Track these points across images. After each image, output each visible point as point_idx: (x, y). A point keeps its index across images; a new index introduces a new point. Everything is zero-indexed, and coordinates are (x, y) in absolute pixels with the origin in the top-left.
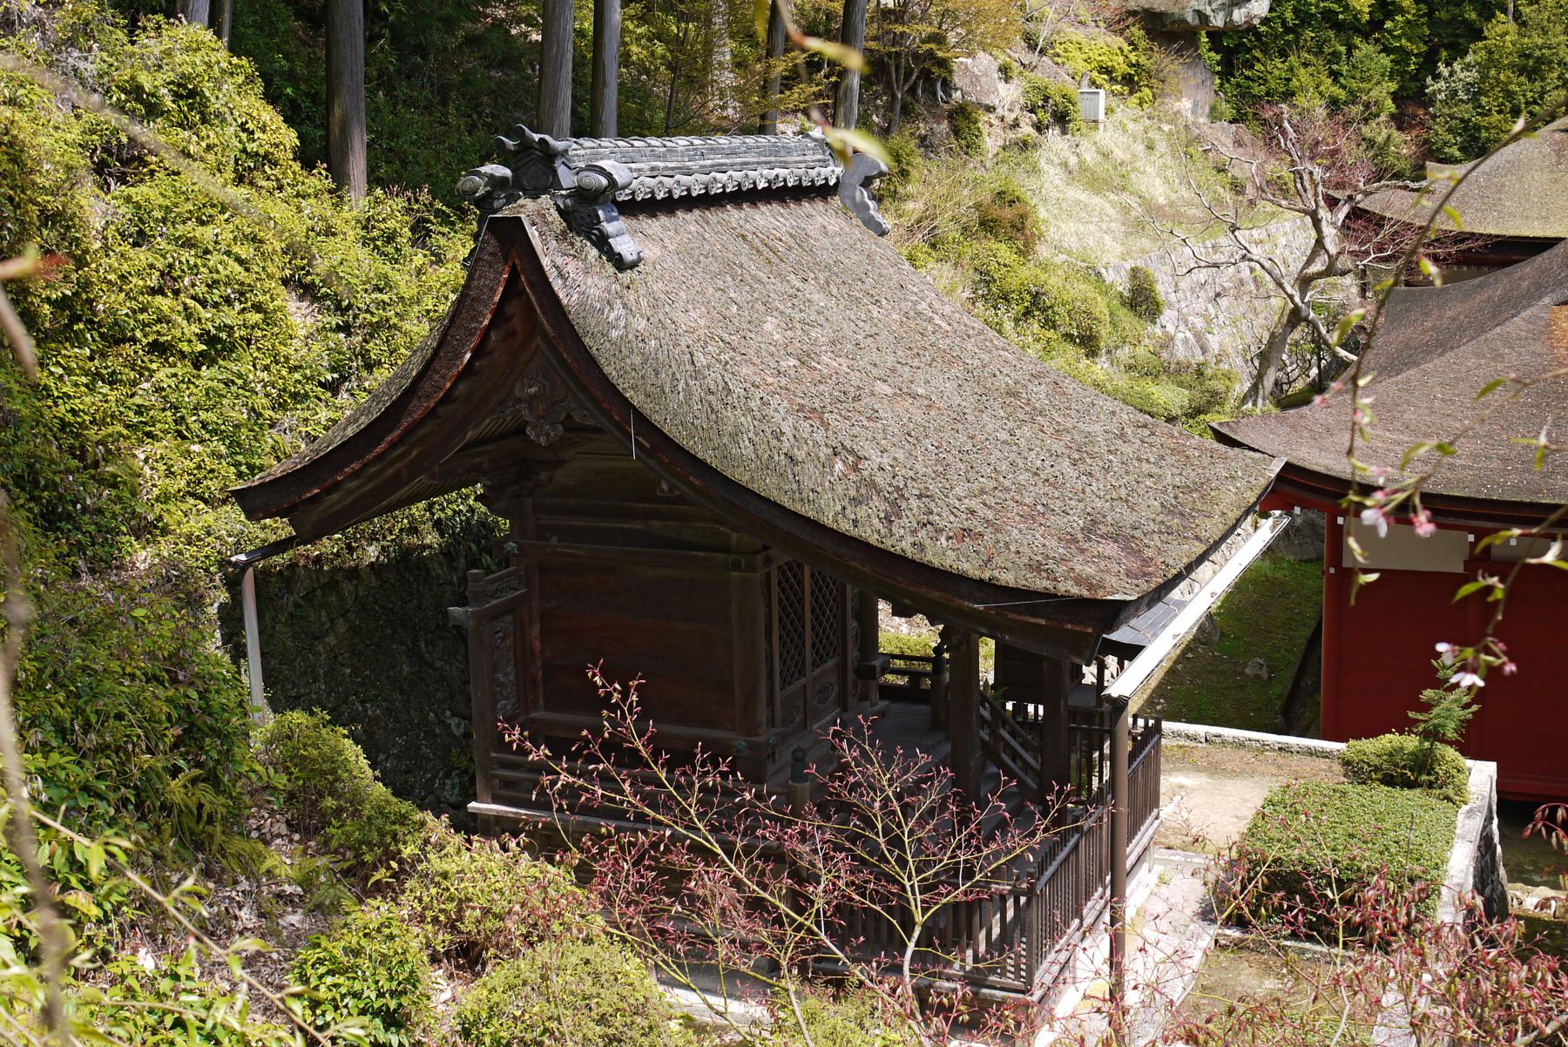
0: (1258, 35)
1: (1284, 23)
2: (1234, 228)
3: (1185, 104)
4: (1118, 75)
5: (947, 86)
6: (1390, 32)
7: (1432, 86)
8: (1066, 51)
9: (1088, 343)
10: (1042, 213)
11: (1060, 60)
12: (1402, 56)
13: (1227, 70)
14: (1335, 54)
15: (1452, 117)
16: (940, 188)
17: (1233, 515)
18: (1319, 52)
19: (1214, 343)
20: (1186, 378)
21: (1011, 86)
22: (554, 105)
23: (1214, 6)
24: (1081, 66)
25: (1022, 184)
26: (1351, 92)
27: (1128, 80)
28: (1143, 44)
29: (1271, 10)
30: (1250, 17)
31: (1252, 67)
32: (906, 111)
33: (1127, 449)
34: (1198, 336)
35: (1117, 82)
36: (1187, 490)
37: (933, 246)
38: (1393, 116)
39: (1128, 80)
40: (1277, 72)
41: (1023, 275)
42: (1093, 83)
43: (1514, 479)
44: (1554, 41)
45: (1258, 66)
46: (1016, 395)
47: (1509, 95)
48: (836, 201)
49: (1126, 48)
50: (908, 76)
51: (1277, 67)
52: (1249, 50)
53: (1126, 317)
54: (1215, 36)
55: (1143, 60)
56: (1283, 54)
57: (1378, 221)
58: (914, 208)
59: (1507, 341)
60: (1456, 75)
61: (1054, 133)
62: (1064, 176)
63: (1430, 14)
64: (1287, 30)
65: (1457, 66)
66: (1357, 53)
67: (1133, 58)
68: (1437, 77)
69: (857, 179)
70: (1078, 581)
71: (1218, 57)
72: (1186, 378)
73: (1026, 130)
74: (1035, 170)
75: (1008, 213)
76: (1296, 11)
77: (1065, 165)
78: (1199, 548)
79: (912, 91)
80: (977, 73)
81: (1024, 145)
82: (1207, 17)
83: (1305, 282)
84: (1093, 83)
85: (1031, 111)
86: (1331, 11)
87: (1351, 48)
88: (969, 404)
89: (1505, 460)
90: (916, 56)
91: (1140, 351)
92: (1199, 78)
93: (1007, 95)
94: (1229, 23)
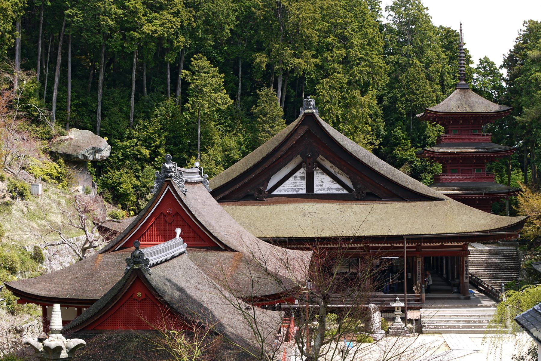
0: (109, 162)
1: (118, 158)
2: (60, 234)
4: (54, 176)
6: (157, 162)
8: (33, 168)
9: (12, 270)
11: (31, 171)
13: (98, 175)
14: (137, 170)
18: (131, 169)
21: (4, 183)
23: (89, 153)
26: (143, 183)
27: (58, 178)
29: (111, 153)
30: (102, 157)
31: (107, 173)
35: (53, 179)
39: (58, 178)
40: (116, 175)
44: (210, 167)
45: (109, 173)
49: (57, 166)
51: (116, 174)
52: (106, 167)
53: (31, 263)
55: (63, 171)
56: (119, 169)
57: (107, 230)
61: (19, 200)
62: (21, 215)
64: (120, 160)
66: (146, 169)
67: (59, 170)
71: (95, 169)
73: (8, 199)
74: (10, 213)
76: (122, 154)
77: (22, 211)
81: (7, 204)
82: (86, 157)
83: (84, 250)
85: (10, 192)
86: (135, 154)
87: (143, 168)
89: (74, 290)
92: (85, 178)
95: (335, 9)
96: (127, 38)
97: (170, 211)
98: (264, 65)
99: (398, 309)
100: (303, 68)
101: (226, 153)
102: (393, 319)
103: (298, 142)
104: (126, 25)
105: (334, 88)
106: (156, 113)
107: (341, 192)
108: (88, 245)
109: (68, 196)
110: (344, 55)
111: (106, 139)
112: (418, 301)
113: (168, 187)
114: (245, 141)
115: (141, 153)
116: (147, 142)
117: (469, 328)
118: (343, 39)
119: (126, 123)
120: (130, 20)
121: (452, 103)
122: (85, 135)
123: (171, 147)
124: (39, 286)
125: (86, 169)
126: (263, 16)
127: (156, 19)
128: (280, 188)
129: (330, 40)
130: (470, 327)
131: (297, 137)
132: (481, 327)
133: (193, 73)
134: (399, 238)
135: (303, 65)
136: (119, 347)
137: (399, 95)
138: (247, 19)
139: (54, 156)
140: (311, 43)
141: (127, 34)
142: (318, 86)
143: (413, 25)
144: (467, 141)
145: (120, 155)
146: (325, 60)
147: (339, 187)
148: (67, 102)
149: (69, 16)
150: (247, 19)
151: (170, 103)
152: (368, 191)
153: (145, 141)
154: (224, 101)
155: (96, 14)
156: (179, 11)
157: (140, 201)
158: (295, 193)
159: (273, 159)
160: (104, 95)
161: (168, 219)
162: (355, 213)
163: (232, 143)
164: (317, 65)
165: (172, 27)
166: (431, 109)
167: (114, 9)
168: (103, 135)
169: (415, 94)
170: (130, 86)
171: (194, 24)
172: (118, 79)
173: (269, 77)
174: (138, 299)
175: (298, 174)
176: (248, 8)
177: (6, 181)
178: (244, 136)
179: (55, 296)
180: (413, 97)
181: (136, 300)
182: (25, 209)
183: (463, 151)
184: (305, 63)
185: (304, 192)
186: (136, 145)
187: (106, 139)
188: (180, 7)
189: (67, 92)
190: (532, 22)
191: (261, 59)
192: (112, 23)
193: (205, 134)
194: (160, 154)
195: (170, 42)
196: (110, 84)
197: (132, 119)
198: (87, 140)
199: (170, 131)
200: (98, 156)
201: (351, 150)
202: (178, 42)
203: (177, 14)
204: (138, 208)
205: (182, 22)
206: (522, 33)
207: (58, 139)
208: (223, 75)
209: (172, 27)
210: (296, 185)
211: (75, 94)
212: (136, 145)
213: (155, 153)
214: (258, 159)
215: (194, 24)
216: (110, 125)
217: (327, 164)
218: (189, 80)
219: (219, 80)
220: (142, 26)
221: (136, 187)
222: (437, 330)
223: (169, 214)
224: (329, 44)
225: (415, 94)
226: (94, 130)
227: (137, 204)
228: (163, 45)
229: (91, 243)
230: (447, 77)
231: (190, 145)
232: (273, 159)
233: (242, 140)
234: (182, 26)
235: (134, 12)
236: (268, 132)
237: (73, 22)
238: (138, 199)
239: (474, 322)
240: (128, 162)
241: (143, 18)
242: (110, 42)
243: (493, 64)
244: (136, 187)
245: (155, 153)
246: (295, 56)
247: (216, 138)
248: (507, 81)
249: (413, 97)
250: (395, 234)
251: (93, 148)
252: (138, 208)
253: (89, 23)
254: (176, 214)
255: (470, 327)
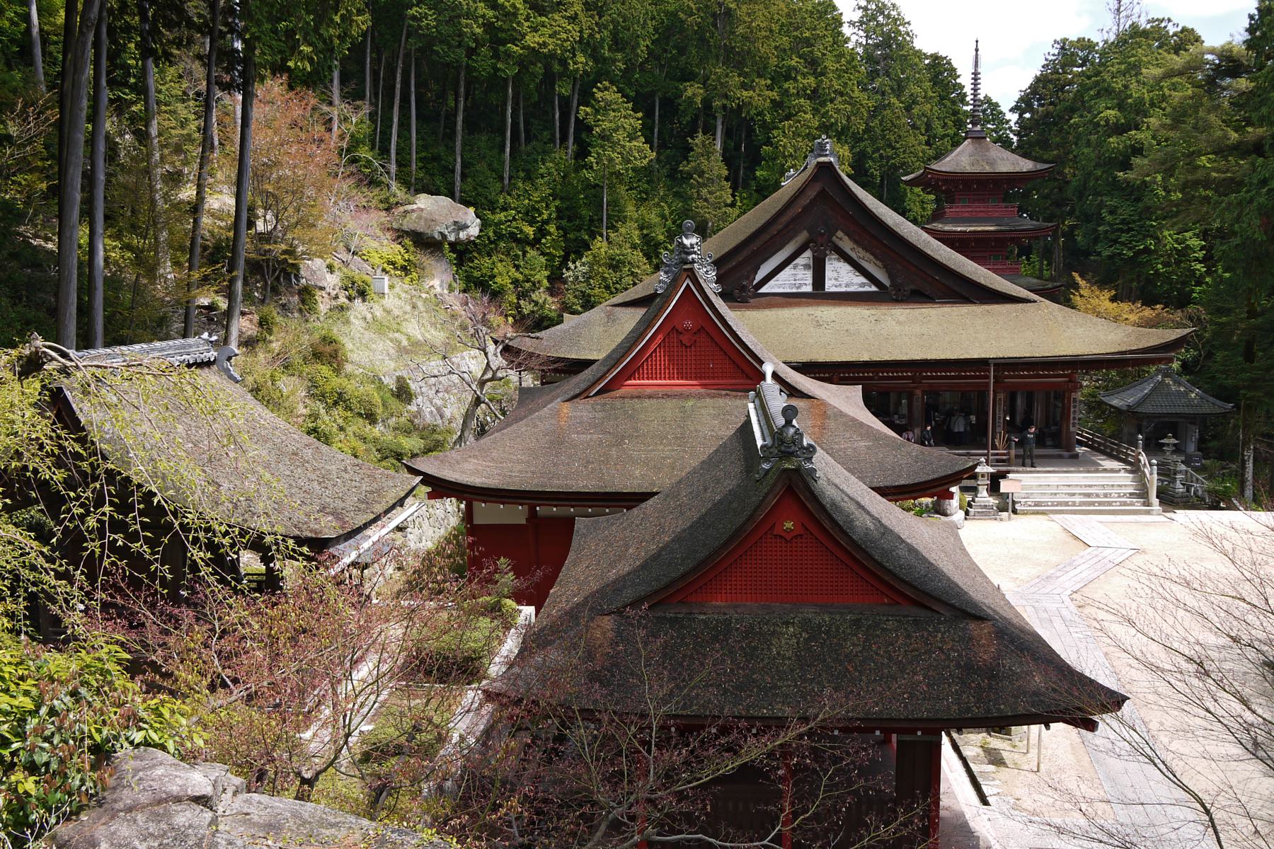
1: (489, 238)
3: (436, 283)
5: (297, 277)
7: (566, 274)
9: (371, 418)
10: (349, 346)
12: (550, 257)
14: (517, 256)
15: (576, 290)
16: (290, 334)
17: (391, 503)
18: (508, 255)
19: (448, 413)
20: (426, 433)
22: (67, 302)
24: (377, 261)
25: (336, 331)
27: (404, 268)
28: (412, 249)
29: (481, 231)
32: (275, 291)
33: (347, 476)
34: (438, 409)
36: (372, 492)
37: (286, 367)
38: (548, 289)
39: (404, 268)
41: (336, 382)
42: (384, 270)
43: (536, 481)
46: (296, 454)
47: (604, 279)
48: (215, 368)
49: (403, 251)
50: (274, 270)
51: (487, 262)
53: (394, 404)
54: (453, 246)
55: (412, 258)
56: (490, 255)
57: (518, 352)
58: (276, 346)
59: (540, 419)
60: (577, 269)
61: (358, 301)
62: (364, 325)
63: (564, 236)
64: (491, 242)
65: (578, 264)
67: (406, 256)
68: (568, 269)
69: (225, 357)
70: (311, 531)
72: (426, 433)
73: (343, 300)
74: (348, 322)
75: (328, 349)
76: (495, 232)
78: (372, 516)
79: (278, 279)
80: (314, 269)
81: (341, 308)
83: (482, 383)
84: (384, 270)
87: (525, 253)
88: (273, 459)
89: (533, 473)
90: (278, 262)
91: (403, 420)
92: (444, 267)
93: (332, 281)
94: (458, 238)
95: (798, 17)
96: (502, 55)
97: (688, 324)
98: (698, 100)
99: (983, 476)
100: (224, 237)
101: (645, 232)
102: (974, 490)
103: (806, 209)
104: (497, 36)
105: (799, 135)
106: (541, 171)
107: (867, 289)
108: (489, 375)
109: (424, 296)
110: (814, 85)
111: (472, 210)
112: (1003, 461)
113: (688, 281)
114: (671, 214)
115: (521, 231)
116: (529, 215)
117: (1092, 506)
118: (813, 63)
119: (498, 185)
120: (505, 27)
121: (961, 159)
122: (441, 203)
123: (564, 223)
124: (466, 466)
125: (444, 256)
126: (698, 24)
127: (543, 26)
128: (772, 282)
129: (793, 63)
130: (1092, 504)
131: (804, 201)
132: (1110, 504)
133: (597, 111)
134: (982, 363)
135: (758, 101)
136: (755, 648)
137: (869, 150)
138: (670, 29)
139: (400, 235)
140: (765, 68)
141: (502, 48)
142: (775, 132)
143: (890, 45)
144: (981, 215)
145: (491, 234)
146: (786, 93)
147: (865, 280)
148: (410, 154)
149: (414, 18)
150: (670, 29)
151: (564, 155)
152: (912, 287)
153: (527, 214)
154: (642, 153)
155: (455, 15)
156: (576, 14)
157: (522, 302)
158: (794, 290)
159: (766, 237)
160: (464, 144)
161: (685, 339)
162: (899, 323)
163: (653, 218)
164: (773, 101)
165: (568, 40)
166: (933, 167)
167: (482, 8)
168: (467, 204)
169: (893, 148)
170: (503, 134)
171: (598, 36)
172: (483, 119)
173: (704, 119)
174: (783, 534)
175: (801, 261)
176: (674, 14)
177: (337, 273)
178: (670, 207)
179: (501, 487)
180: (890, 152)
181: (781, 537)
182: (369, 316)
183: (979, 229)
184: (759, 96)
185: (809, 289)
186: (514, 219)
187: (472, 210)
188: (578, 8)
189: (410, 138)
190: (1064, 41)
191: (693, 91)
192: (478, 31)
193: (614, 203)
194: (550, 234)
195: (563, 62)
196: (471, 126)
197: (506, 182)
198: (445, 211)
199: (561, 199)
200: (463, 235)
201: (890, 222)
202: (575, 63)
203: (573, 19)
204: (519, 312)
205: (581, 32)
206: (1051, 58)
207: (401, 209)
208: (640, 115)
209: (568, 40)
210: (796, 278)
211: (421, 142)
212: (514, 219)
213: (542, 232)
214: (742, 237)
215: (598, 36)
216: (475, 189)
217: (847, 245)
218: (591, 120)
219: (634, 121)
220: (524, 36)
221: (515, 282)
222: (1039, 510)
223: (687, 330)
224: (790, 68)
225: (893, 148)
226: (451, 195)
227: (518, 306)
228: (550, 66)
229: (495, 373)
230: (937, 124)
231: (591, 220)
232: (766, 237)
233: (667, 212)
234: (581, 37)
235: (512, 15)
236: (706, 200)
237: (420, 27)
238: (518, 299)
239: (1097, 495)
240: (502, 244)
241: (526, 24)
242: (476, 61)
243: (997, 105)
244: (515, 282)
245: (542, 232)
246: (744, 86)
247: (630, 210)
248: (1017, 134)
249: (890, 152)
250: (976, 356)
251: (456, 223)
252: (519, 312)
253: (445, 29)
254: (701, 330)
255: (1092, 504)
